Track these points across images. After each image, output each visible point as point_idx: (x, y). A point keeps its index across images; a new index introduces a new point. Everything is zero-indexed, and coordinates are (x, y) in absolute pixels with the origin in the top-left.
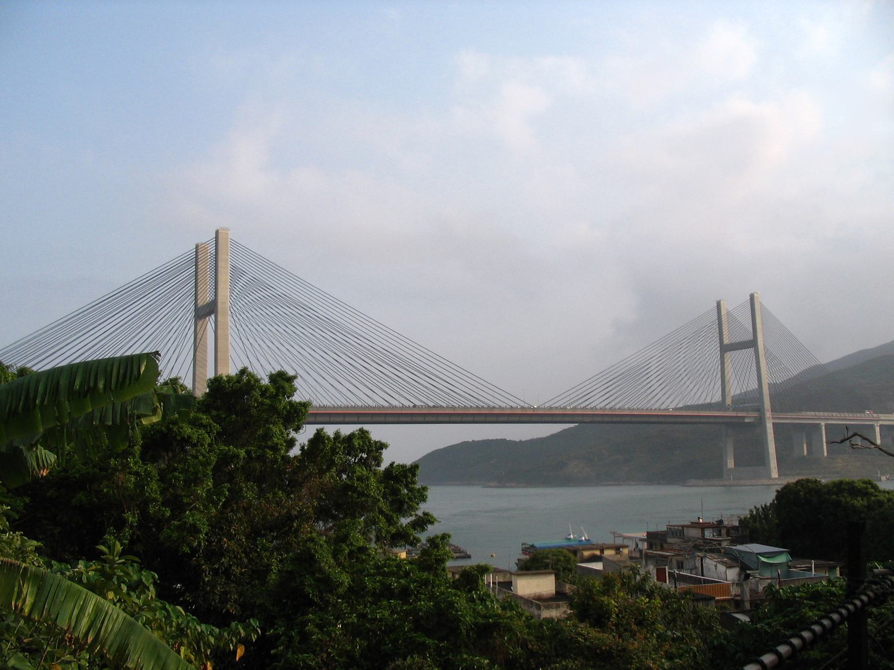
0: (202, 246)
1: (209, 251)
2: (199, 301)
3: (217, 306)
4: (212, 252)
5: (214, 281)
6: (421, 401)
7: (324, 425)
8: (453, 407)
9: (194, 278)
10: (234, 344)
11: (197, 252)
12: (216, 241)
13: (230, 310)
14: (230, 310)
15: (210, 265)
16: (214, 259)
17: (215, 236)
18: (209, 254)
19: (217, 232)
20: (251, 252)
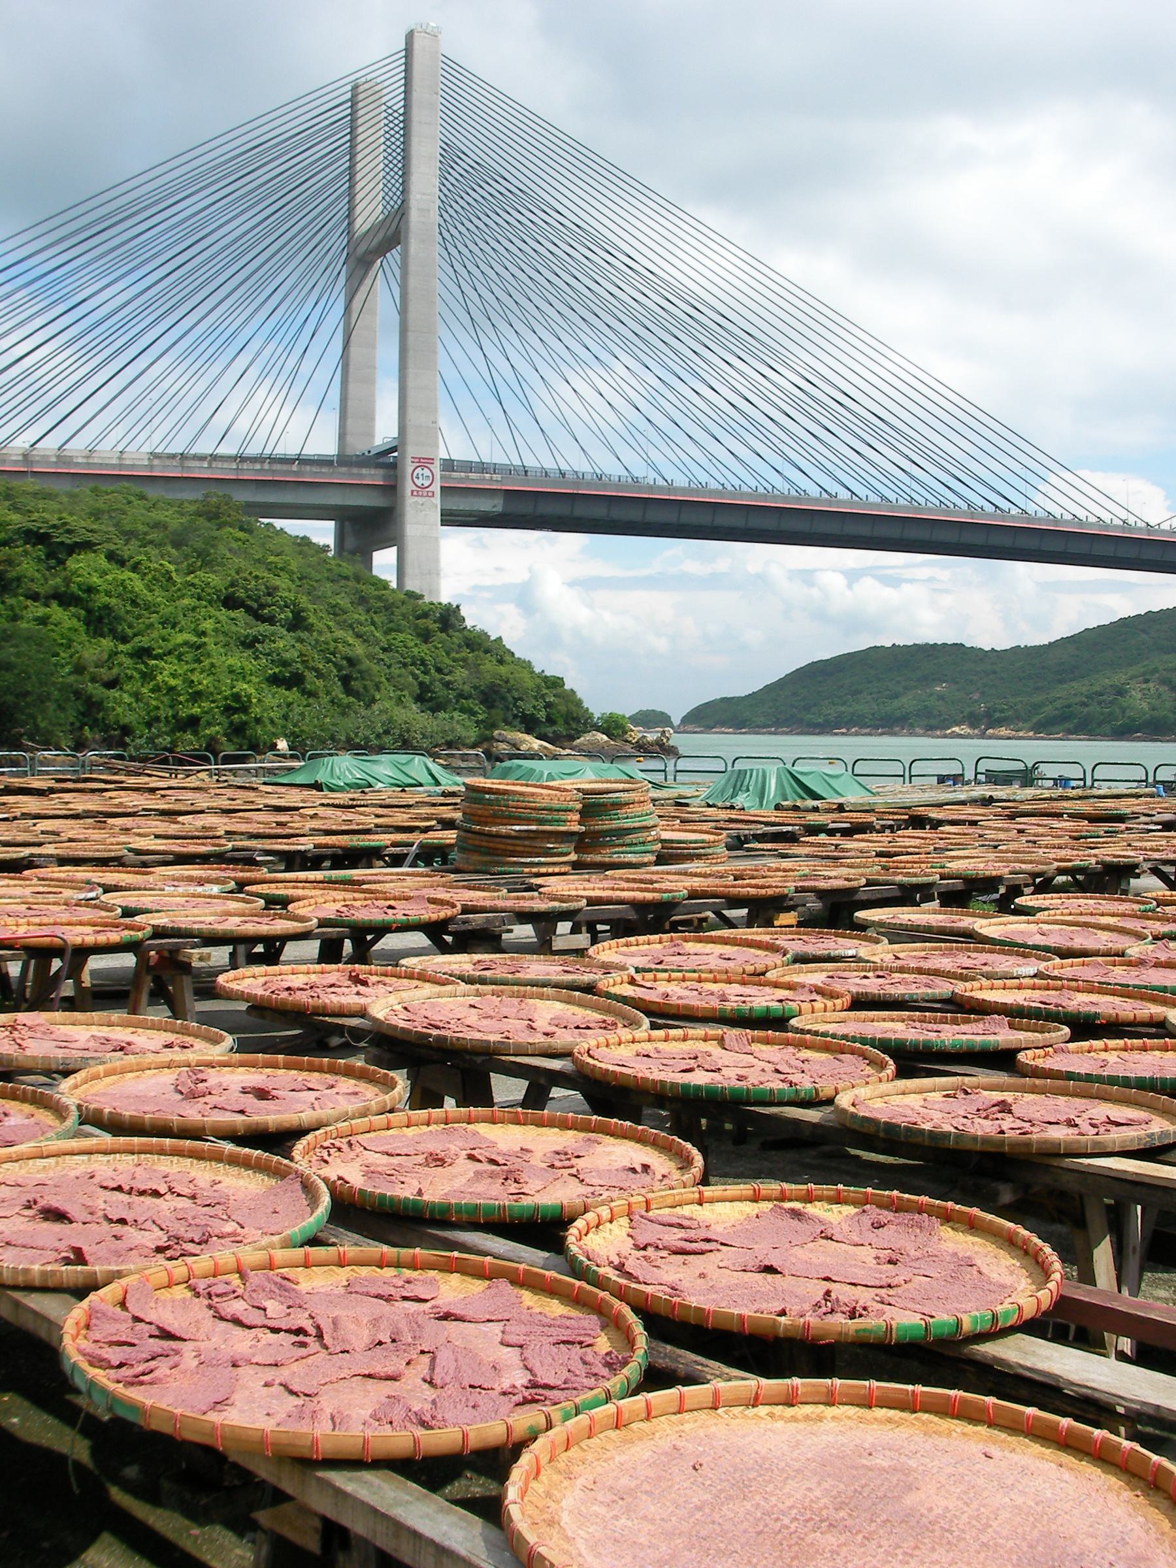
0: (366, 86)
1: (384, 100)
2: (358, 222)
3: (407, 222)
4: (395, 108)
5: (399, 158)
6: (876, 491)
7: (725, 1029)
8: (670, 487)
9: (347, 199)
10: (446, 296)
11: (354, 102)
12: (406, 57)
13: (441, 234)
14: (441, 234)
15: (388, 136)
16: (401, 125)
17: (403, 47)
18: (384, 107)
19: (410, 37)
20: (557, 870)
